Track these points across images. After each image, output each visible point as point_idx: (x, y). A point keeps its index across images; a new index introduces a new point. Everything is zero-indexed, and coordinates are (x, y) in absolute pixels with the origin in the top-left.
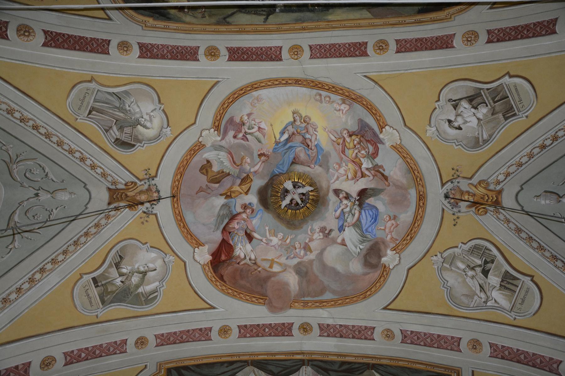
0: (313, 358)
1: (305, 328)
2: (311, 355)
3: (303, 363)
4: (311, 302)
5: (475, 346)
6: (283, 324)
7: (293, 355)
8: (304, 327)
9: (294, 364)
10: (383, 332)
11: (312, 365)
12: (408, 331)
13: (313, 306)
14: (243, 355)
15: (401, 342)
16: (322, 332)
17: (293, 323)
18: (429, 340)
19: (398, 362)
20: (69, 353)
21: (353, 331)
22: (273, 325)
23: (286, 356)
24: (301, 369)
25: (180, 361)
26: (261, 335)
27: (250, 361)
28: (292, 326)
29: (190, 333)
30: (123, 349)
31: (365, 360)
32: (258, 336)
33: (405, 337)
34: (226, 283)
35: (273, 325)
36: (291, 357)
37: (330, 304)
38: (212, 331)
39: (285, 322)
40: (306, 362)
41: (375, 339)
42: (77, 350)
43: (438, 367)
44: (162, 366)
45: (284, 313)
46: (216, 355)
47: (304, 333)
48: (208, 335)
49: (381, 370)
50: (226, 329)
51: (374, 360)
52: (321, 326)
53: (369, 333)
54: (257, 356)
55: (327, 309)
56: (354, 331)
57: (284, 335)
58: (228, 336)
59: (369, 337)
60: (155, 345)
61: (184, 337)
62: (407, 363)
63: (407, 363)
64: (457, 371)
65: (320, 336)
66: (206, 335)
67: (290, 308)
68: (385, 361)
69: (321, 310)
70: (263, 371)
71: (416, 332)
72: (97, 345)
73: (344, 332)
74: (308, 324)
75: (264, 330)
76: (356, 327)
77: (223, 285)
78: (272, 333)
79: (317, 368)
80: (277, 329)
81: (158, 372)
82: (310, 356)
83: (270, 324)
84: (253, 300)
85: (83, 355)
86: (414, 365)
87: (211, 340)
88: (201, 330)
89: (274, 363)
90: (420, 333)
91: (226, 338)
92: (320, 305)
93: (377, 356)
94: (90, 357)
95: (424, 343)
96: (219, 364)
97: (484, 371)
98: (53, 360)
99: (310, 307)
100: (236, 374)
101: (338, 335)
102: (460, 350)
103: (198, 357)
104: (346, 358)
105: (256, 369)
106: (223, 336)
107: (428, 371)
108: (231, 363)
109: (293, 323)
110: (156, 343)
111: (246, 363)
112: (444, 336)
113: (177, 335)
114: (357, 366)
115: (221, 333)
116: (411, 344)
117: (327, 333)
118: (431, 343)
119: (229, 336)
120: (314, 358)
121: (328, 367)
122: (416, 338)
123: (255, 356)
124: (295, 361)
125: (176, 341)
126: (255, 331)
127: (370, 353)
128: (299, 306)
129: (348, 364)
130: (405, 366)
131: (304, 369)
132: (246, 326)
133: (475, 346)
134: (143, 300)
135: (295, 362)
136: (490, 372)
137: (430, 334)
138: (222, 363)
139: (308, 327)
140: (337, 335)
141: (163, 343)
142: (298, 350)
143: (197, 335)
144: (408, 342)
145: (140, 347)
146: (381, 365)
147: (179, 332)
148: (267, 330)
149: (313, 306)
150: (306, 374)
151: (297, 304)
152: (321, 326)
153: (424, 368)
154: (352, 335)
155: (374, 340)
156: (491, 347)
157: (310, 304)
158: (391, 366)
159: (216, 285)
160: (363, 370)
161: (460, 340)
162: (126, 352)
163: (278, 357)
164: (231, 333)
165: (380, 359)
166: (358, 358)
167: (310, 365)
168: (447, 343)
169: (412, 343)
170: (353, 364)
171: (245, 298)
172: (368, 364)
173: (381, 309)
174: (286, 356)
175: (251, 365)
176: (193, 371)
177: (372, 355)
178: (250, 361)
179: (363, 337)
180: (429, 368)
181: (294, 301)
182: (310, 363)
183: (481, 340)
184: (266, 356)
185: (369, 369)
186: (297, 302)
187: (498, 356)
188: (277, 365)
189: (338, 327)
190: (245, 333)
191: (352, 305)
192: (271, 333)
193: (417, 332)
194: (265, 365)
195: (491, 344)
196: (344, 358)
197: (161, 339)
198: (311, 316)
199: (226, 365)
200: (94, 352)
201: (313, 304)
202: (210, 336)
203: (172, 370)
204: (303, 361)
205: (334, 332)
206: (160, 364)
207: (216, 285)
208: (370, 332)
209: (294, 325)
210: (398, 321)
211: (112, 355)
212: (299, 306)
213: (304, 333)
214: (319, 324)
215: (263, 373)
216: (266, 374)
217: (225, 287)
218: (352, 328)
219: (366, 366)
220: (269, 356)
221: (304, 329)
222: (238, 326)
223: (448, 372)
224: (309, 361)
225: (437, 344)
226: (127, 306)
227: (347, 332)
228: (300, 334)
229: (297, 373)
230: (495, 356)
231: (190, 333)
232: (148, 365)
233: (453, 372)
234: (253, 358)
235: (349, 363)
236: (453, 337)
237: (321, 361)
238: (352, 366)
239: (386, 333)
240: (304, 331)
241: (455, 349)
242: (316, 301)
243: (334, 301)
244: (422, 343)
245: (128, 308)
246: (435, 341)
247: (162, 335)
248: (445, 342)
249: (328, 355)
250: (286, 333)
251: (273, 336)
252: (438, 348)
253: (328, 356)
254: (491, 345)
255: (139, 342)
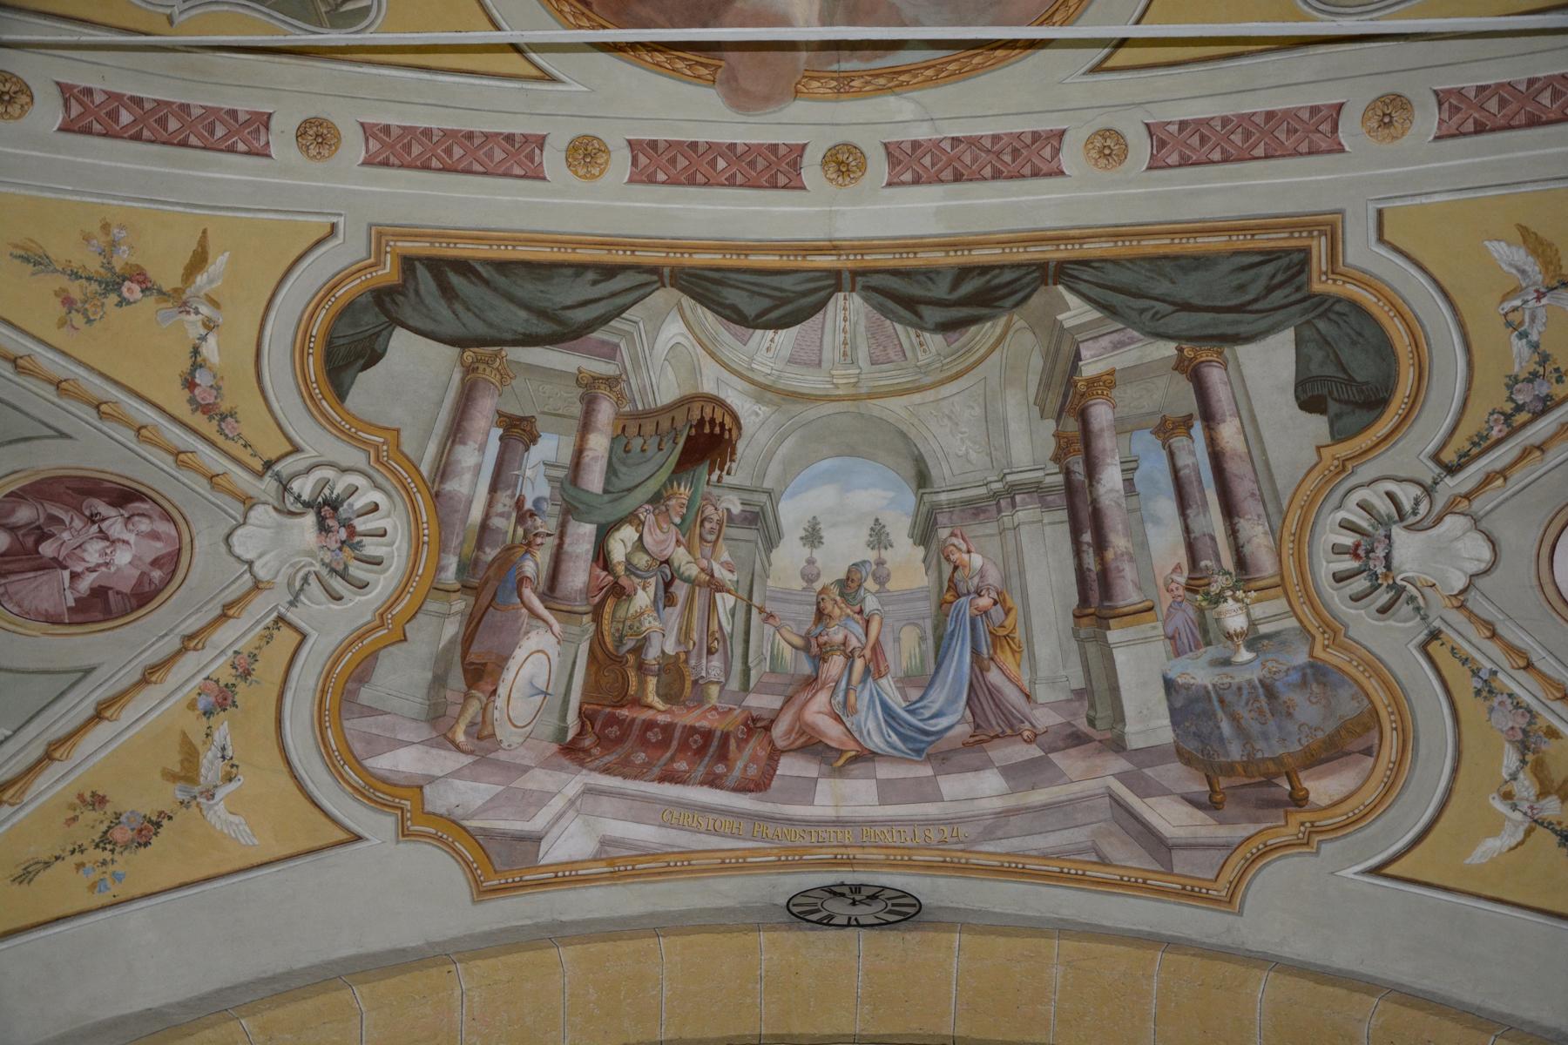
0: (868, 264)
1: (844, 163)
2: (862, 255)
3: (835, 281)
4: (862, 77)
5: (1390, 115)
6: (774, 148)
7: (804, 256)
8: (840, 157)
9: (812, 285)
10: (1089, 141)
11: (866, 288)
12: (1169, 123)
13: (867, 88)
14: (645, 246)
15: (1150, 168)
16: (898, 169)
17: (804, 146)
18: (1237, 138)
19: (1139, 241)
20: (76, 91)
21: (994, 153)
22: (739, 150)
23: (781, 256)
24: (831, 305)
25: (443, 236)
26: (704, 180)
27: (666, 271)
28: (801, 156)
29: (477, 142)
30: (258, 140)
31: (1034, 253)
32: (692, 182)
33: (1162, 144)
34: (591, 10)
35: (739, 150)
36: (799, 263)
37: (921, 78)
38: (547, 148)
39: (780, 142)
40: (846, 277)
41: (1065, 170)
42: (105, 92)
43: (1265, 228)
44: (387, 242)
45: (775, 112)
46: (559, 237)
47: (840, 179)
48: (532, 161)
49: (1085, 281)
50: (590, 148)
51: (1062, 247)
52: (893, 153)
53: (1047, 152)
54: (690, 254)
55: (915, 94)
56: (998, 154)
57: (774, 186)
58: (596, 171)
59: (1045, 168)
60: (361, 160)
61: (458, 152)
62: (1168, 241)
63: (1168, 241)
64: (1328, 228)
65: (890, 184)
66: (526, 157)
67: (795, 98)
68: (1097, 245)
69: (892, 99)
70: (709, 308)
71: (1194, 121)
72: (173, 103)
73: (967, 159)
74: (852, 148)
75: (713, 163)
76: (1006, 139)
77: (583, 14)
78: (739, 175)
79: (881, 299)
80: (752, 164)
81: (372, 260)
82: (859, 257)
83: (732, 147)
84: (678, 66)
85: (125, 117)
86: (1192, 241)
87: (544, 179)
88: (510, 138)
89: (743, 282)
90: (1207, 122)
91: (590, 177)
92: (890, 85)
93: (1072, 233)
94: (149, 133)
95: (1223, 151)
96: (570, 272)
97: (1418, 201)
98: (21, 91)
99: (860, 94)
100: (623, 311)
101: (947, 174)
102: (1340, 144)
103: (502, 234)
104: (973, 253)
105: (687, 302)
106: (582, 171)
107: (1236, 253)
108: (609, 271)
109: (804, 146)
110: (367, 152)
111: (655, 276)
112: (1286, 112)
113: (435, 139)
114: (1008, 276)
115: (575, 159)
116: (1180, 165)
117: (914, 170)
118: (1245, 146)
119: (602, 172)
120: (872, 264)
121: (917, 291)
122: (1195, 140)
123: (682, 254)
124: (811, 275)
125: (430, 159)
126: (682, 162)
127: (1048, 224)
128: (822, 90)
129: (979, 274)
130: (1161, 251)
131: (841, 302)
132: (653, 144)
133: (1390, 115)
134: (323, 9)
135: (808, 281)
136: (1437, 198)
137: (1241, 117)
138: (580, 268)
139: (851, 159)
140: (943, 176)
141: (388, 158)
142: (822, 236)
143: (499, 155)
144: (1169, 161)
145: (313, 152)
146: (1085, 263)
147: (441, 134)
148: (721, 164)
149: (867, 88)
150: (845, 320)
151: (815, 84)
152: (893, 153)
153: (1222, 247)
154: (993, 167)
155: (1062, 173)
156: (1440, 104)
157: (856, 83)
158: (1115, 262)
159: (561, 12)
160: (1029, 290)
161: (1338, 113)
162: (269, 156)
163: (757, 260)
164: (607, 162)
165: (1082, 239)
166: (1011, 248)
167: (858, 287)
168: (1296, 131)
169: (1185, 162)
170: (997, 271)
171: (652, 57)
172: (1042, 266)
173: (1084, 74)
174: (781, 256)
175: (672, 286)
176: (486, 282)
177: (1055, 229)
178: (666, 271)
179: (1027, 170)
180: (1240, 242)
181: (807, 74)
182: (860, 281)
183: (1406, 93)
184: (720, 256)
185: (1046, 284)
186: (817, 79)
187: (1464, 129)
188: (756, 289)
189: (947, 146)
190: (652, 169)
191: (990, 72)
192: (734, 176)
193: (1199, 122)
194: (714, 287)
195: (1441, 95)
196: (966, 253)
197: (383, 144)
198: (861, 121)
199: (590, 276)
200: (160, 118)
201: (867, 83)
202: (541, 163)
203: (417, 264)
204: (836, 274)
205: (933, 165)
206: (380, 235)
207: (561, 12)
208: (1048, 148)
209: (808, 151)
210: (1137, 100)
211: (221, 151)
212: (822, 90)
213: (840, 179)
214: (886, 145)
215: (709, 314)
216: (720, 318)
217: (589, 19)
218: (992, 143)
219: (1035, 275)
220: (728, 256)
221: (840, 163)
222: (629, 142)
223: (1300, 237)
224: (855, 274)
225: (1266, 144)
226: (269, 15)
227: (975, 160)
228: (828, 183)
229: (819, 316)
230: (1453, 131)
231: (477, 142)
232: (341, 226)
233: (1315, 233)
234: (675, 258)
235: (984, 269)
236: (1316, 106)
237: (895, 272)
238: (989, 281)
239: (1098, 143)
240: (839, 170)
241: (1324, 146)
242: (878, 72)
243: (934, 66)
244: (1216, 156)
245: (272, 21)
246: (1258, 135)
247: (387, 129)
248: (1291, 131)
249: (916, 250)
250: (782, 180)
251: (741, 186)
252: (1267, 157)
253: (915, 253)
254: (1441, 97)
255: (311, 132)
